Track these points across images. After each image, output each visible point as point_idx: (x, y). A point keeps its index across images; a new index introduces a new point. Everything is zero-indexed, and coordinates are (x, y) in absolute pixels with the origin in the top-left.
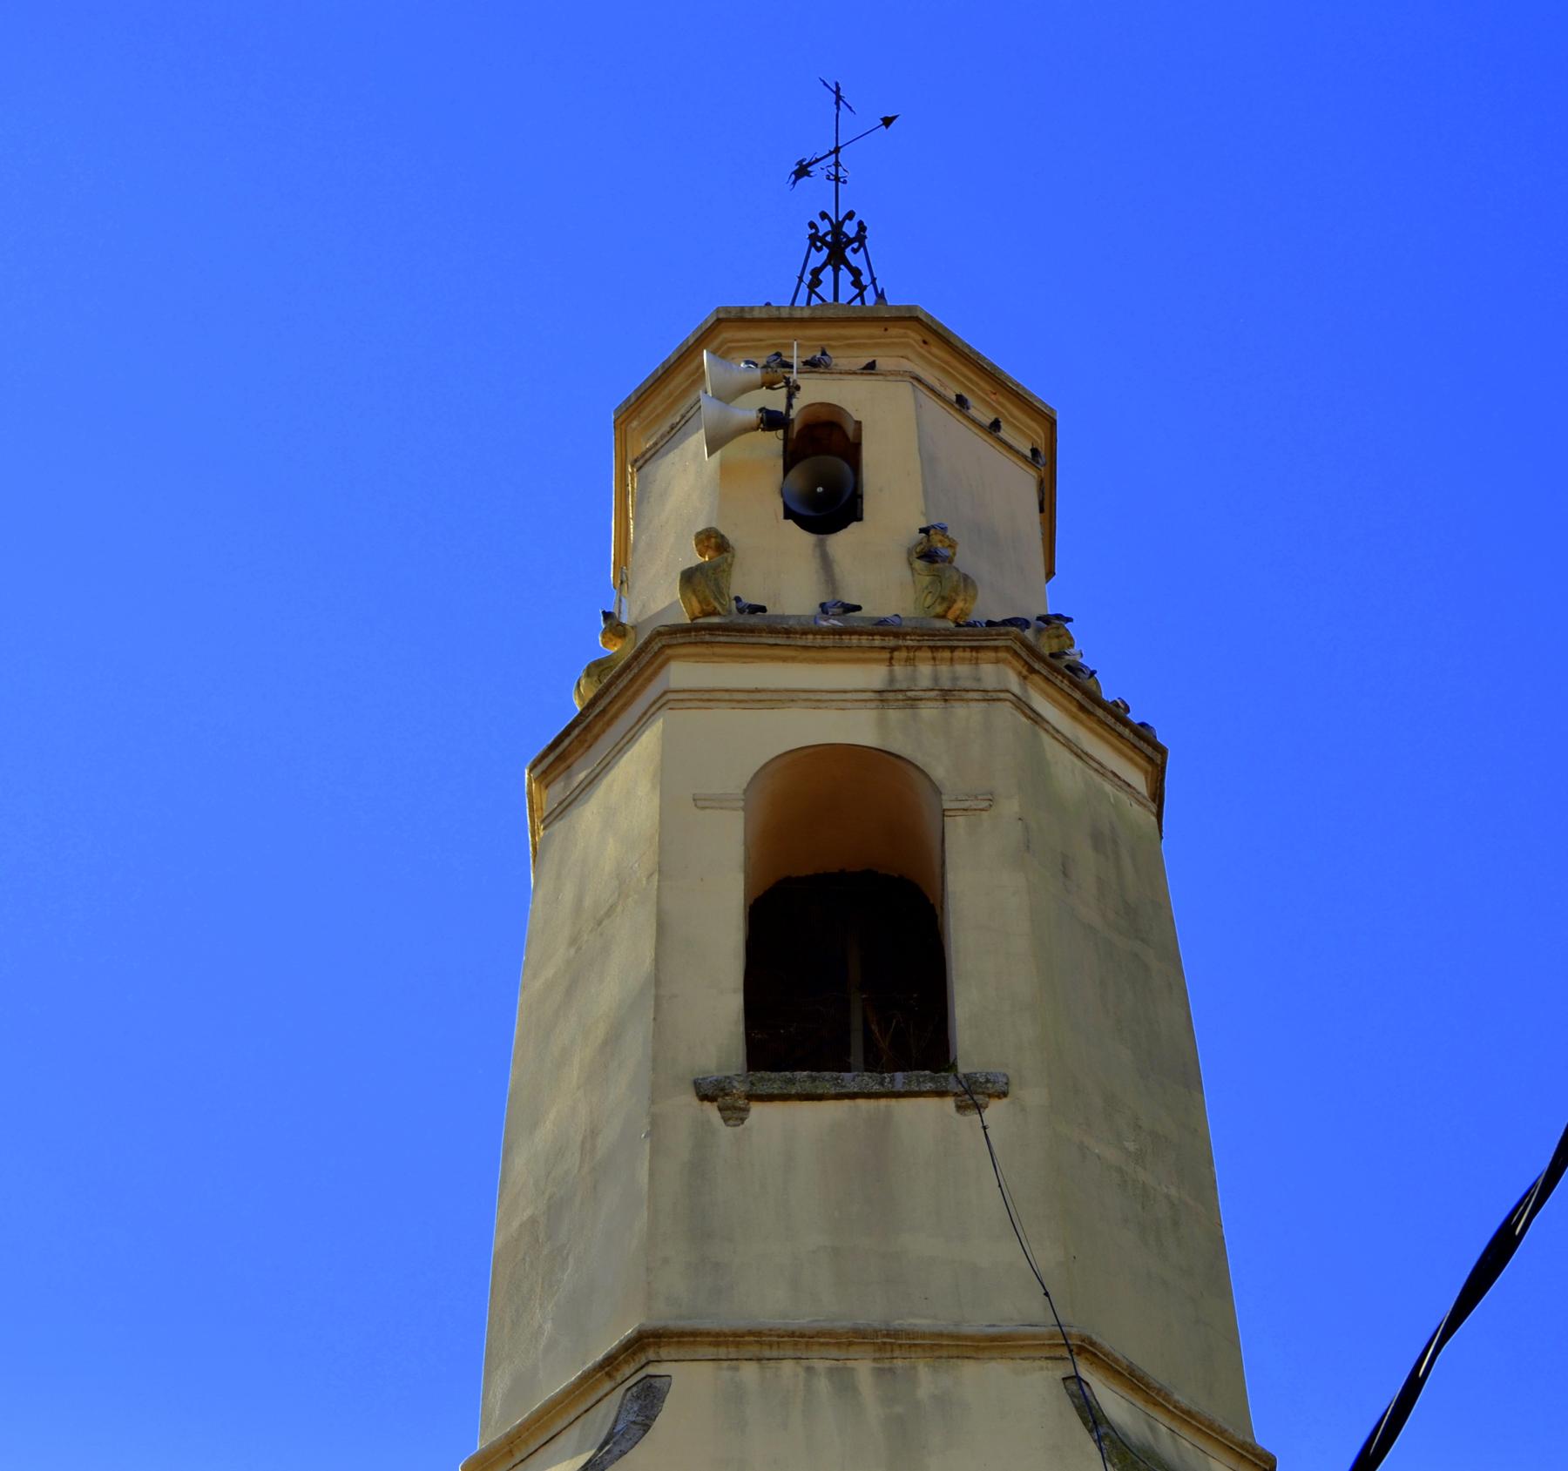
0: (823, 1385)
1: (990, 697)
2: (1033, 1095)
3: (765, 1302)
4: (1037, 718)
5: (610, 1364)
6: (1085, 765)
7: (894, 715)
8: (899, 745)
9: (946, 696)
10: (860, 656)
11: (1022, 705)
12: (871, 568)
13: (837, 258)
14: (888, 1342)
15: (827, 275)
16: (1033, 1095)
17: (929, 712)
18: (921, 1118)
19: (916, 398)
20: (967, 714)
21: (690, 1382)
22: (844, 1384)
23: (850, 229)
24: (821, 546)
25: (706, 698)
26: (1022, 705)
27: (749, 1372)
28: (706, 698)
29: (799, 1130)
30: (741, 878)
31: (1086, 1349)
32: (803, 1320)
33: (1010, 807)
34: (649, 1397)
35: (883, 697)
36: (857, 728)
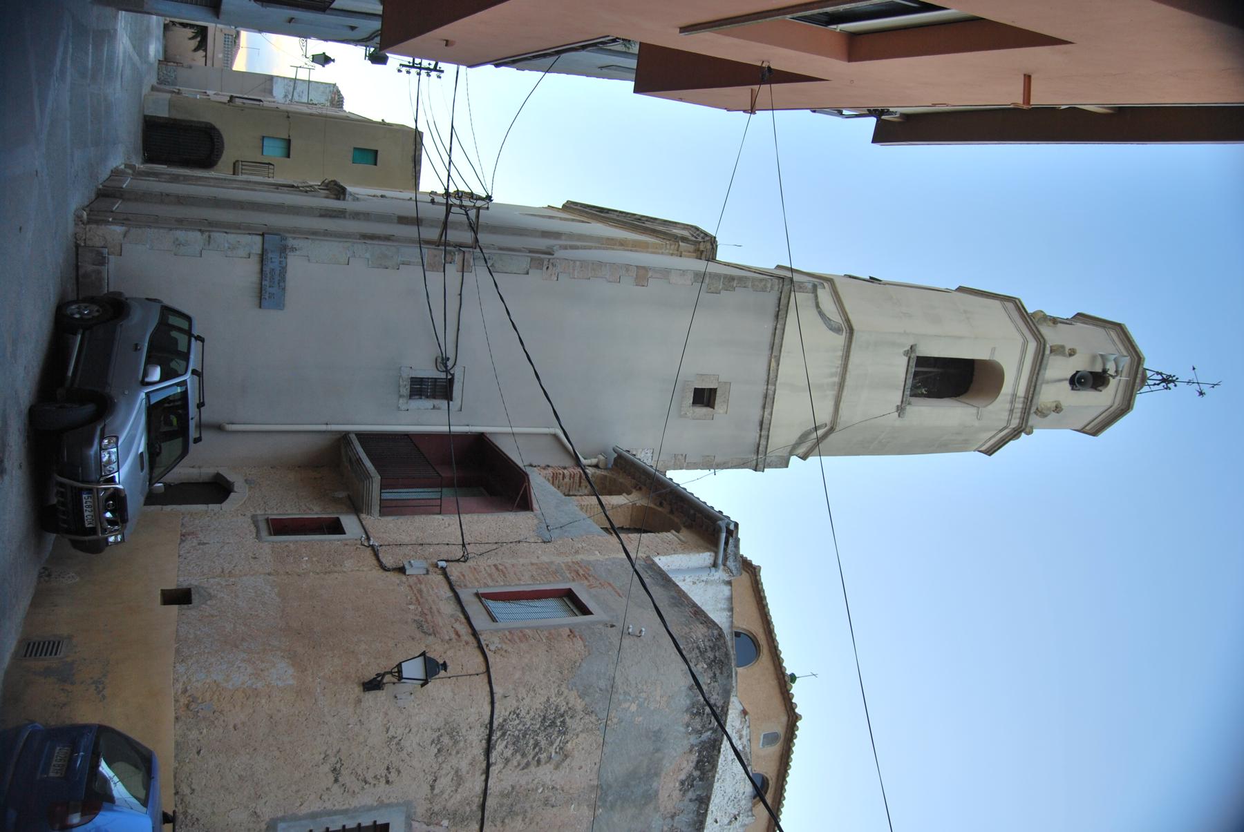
0: (834, 370)
1: (1009, 421)
2: (898, 423)
3: (855, 358)
4: (1001, 431)
5: (848, 321)
6: (988, 438)
7: (1009, 398)
8: (1000, 398)
9: (1011, 411)
10: (1027, 391)
11: (1005, 428)
12: (1055, 391)
13: (1163, 380)
14: (841, 386)
15: (1159, 377)
16: (898, 423)
17: (1008, 406)
18: (896, 397)
19: (486, 608)
20: (1005, 415)
21: (840, 339)
22: (832, 375)
23: (1171, 385)
24: (1048, 382)
25: (1024, 352)
26: (1005, 428)
27: (840, 353)
28: (1024, 352)
29: (899, 368)
30: (483, 517)
31: (832, 430)
32: (850, 366)
33: (977, 424)
34: (838, 330)
35: (1014, 396)
36: (1007, 388)
